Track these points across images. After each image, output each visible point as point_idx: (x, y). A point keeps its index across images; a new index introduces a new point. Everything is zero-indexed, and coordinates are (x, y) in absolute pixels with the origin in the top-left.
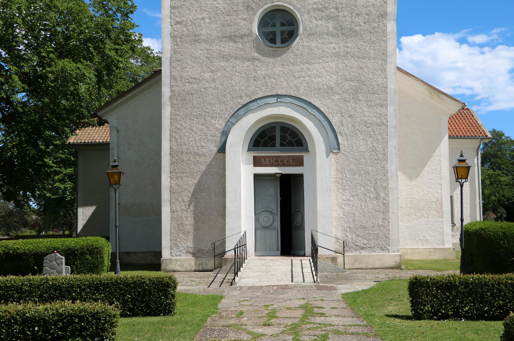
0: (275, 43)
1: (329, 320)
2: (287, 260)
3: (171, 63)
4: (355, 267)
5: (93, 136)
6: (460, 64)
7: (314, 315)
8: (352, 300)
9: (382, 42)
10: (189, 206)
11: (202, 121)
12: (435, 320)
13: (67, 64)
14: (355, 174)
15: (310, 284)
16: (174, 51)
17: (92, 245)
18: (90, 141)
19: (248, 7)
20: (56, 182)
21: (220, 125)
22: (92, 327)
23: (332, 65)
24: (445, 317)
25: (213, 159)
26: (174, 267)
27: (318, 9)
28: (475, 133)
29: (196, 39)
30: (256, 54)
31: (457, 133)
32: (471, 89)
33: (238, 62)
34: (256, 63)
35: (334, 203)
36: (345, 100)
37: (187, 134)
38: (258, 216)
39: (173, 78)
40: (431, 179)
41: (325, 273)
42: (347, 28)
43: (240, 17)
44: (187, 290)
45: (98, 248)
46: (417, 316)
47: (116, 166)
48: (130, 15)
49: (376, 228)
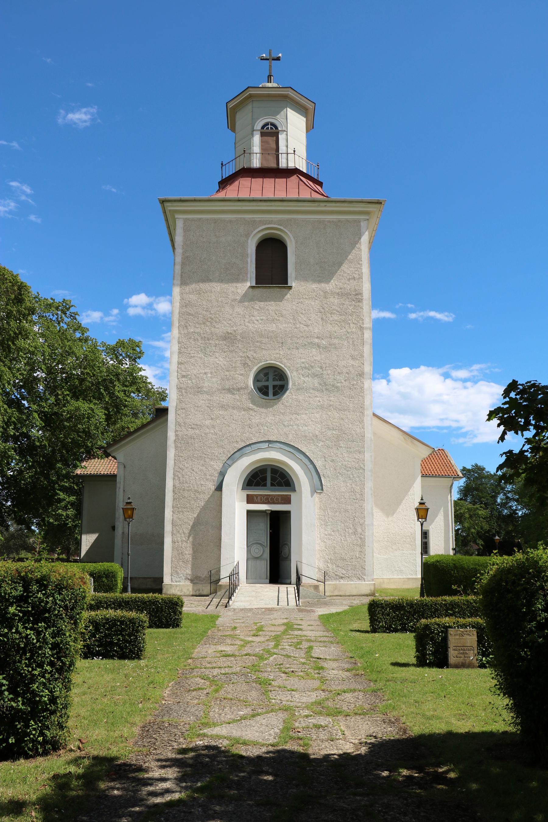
0: (268, 396)
1: (304, 633)
2: (275, 587)
3: (176, 411)
4: (335, 594)
5: (98, 468)
6: (445, 397)
7: (293, 629)
8: (326, 619)
9: (360, 397)
10: (189, 538)
11: (202, 462)
12: (387, 633)
13: (83, 406)
14: (336, 511)
15: (293, 607)
16: (180, 401)
17: (108, 570)
18: (96, 473)
19: (245, 364)
20: (59, 509)
21: (218, 466)
22: (129, 629)
23: (318, 416)
24: (396, 631)
25: (211, 496)
26: (174, 592)
27: (305, 368)
28: (449, 472)
29: (199, 390)
30: (251, 405)
31: (433, 472)
32: (457, 421)
33: (235, 411)
34: (251, 412)
35: (318, 537)
36: (328, 447)
37: (189, 473)
38: (249, 548)
39: (178, 424)
40: (405, 516)
41: (308, 599)
42: (330, 384)
43: (237, 372)
44: (188, 611)
45: (113, 573)
46: (374, 631)
47: (130, 503)
48: (138, 360)
49: (354, 560)
